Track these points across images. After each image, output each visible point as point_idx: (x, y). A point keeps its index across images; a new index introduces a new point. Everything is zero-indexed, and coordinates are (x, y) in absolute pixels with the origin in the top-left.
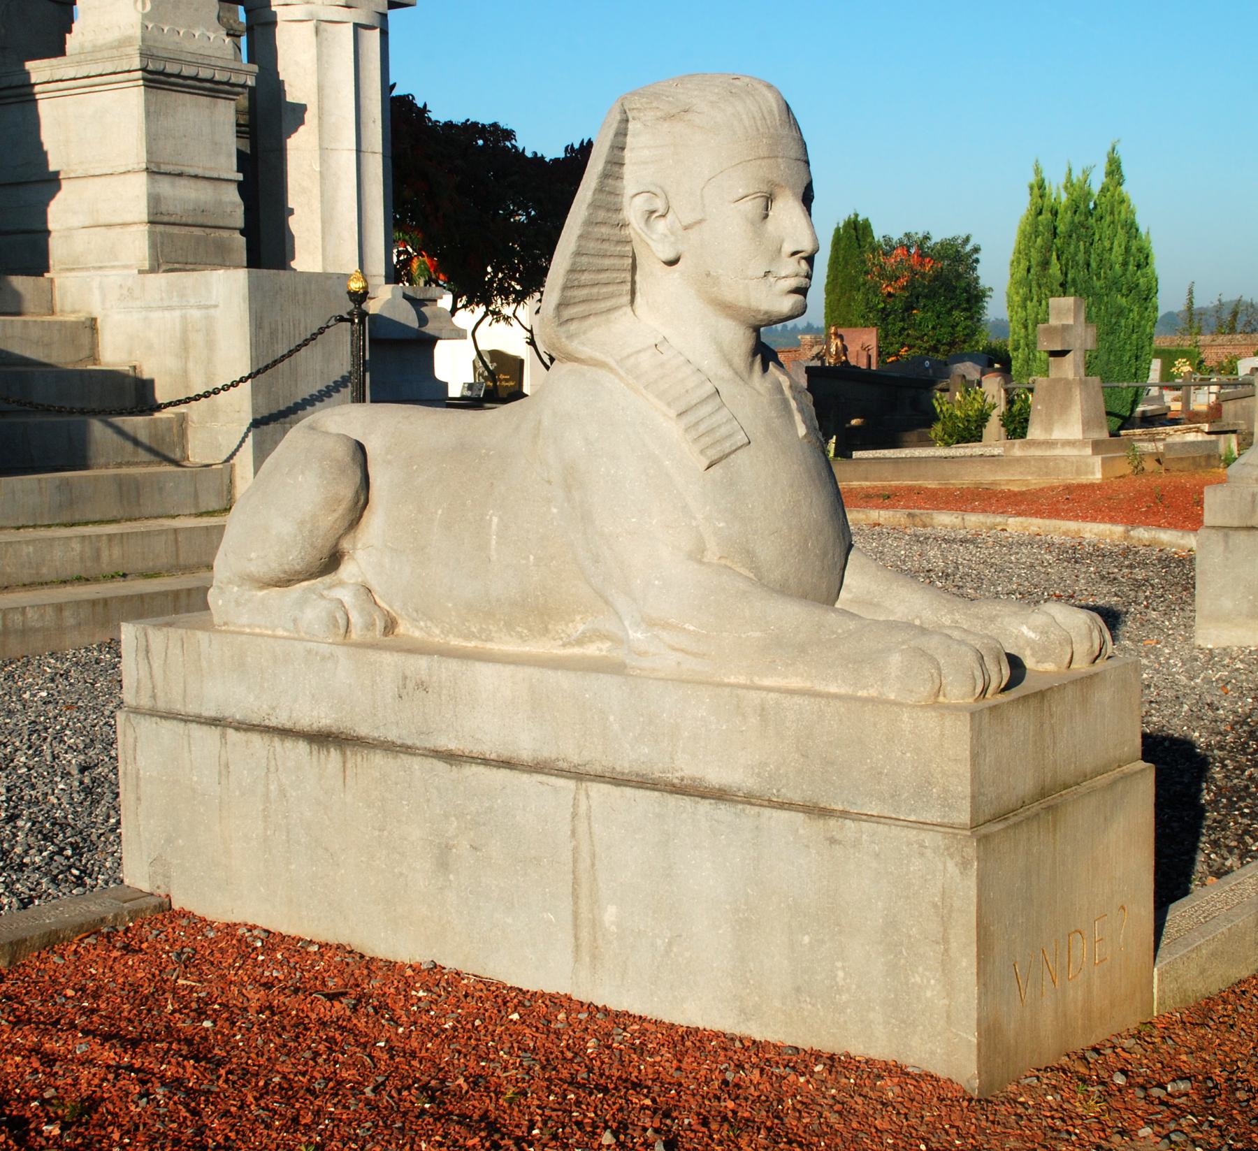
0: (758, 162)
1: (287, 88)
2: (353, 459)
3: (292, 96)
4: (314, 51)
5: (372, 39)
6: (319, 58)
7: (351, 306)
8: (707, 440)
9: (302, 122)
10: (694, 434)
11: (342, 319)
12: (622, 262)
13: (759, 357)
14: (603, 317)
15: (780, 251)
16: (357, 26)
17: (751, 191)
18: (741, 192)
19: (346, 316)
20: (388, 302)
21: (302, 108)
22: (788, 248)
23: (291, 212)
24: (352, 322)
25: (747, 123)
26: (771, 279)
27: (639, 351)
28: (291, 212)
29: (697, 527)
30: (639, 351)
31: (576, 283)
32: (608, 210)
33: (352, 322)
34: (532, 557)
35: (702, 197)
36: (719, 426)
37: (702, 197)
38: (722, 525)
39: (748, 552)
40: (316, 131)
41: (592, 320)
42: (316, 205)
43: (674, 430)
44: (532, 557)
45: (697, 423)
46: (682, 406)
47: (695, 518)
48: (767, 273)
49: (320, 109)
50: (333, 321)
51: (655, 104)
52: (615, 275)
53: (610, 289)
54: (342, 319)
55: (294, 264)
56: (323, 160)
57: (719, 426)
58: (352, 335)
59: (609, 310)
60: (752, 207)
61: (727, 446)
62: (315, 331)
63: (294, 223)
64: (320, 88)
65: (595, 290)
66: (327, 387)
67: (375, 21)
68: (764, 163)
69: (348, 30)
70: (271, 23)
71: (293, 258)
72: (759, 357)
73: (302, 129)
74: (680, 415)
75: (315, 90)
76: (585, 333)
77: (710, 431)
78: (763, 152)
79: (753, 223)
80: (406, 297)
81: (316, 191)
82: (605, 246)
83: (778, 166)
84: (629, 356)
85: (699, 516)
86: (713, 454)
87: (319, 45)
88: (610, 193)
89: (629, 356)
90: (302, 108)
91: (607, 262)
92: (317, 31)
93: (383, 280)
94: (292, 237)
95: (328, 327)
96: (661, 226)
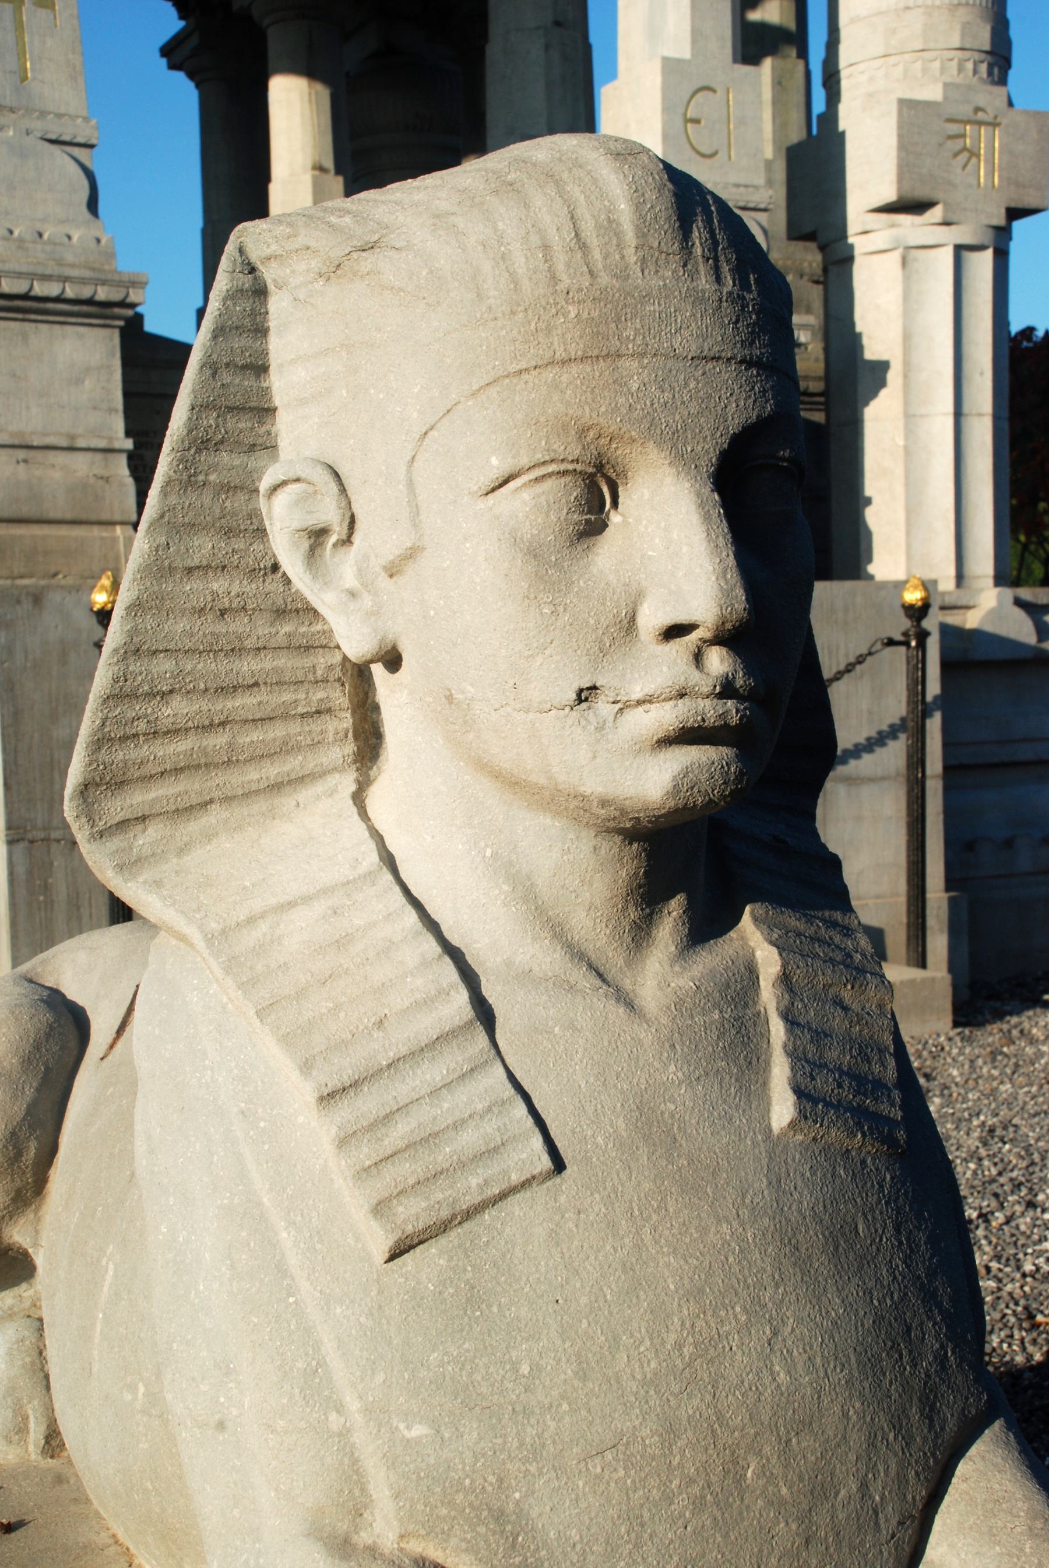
0: (549, 374)
1: (865, 341)
2: (27, 1062)
3: (872, 351)
4: (899, 290)
5: (983, 263)
6: (907, 296)
7: (906, 623)
8: (407, 1170)
9: (882, 384)
10: (365, 1153)
11: (891, 642)
12: (307, 662)
13: (676, 906)
14: (260, 805)
15: (630, 624)
16: (959, 249)
17: (525, 461)
18: (497, 465)
19: (898, 637)
20: (992, 612)
21: (883, 367)
22: (653, 617)
23: (868, 501)
24: (907, 644)
25: (519, 262)
26: (603, 707)
27: (291, 905)
28: (868, 501)
29: (344, 1433)
30: (291, 905)
31: (142, 726)
32: (229, 533)
33: (907, 644)
34: (142, 1389)
35: (410, 484)
36: (458, 1125)
37: (410, 484)
38: (418, 1431)
39: (499, 1516)
40: (901, 394)
41: (215, 815)
42: (900, 490)
43: (315, 1133)
44: (142, 1389)
45: (387, 1118)
46: (342, 1068)
47: (340, 1409)
48: (585, 695)
49: (907, 364)
50: (878, 646)
51: (301, 241)
52: (287, 697)
53: (277, 731)
54: (891, 642)
55: (871, 569)
56: (909, 431)
57: (458, 1125)
58: (908, 662)
59: (276, 787)
60: (537, 507)
61: (472, 1186)
62: (852, 660)
63: (872, 516)
64: (907, 337)
65: (218, 740)
66: (880, 733)
67: (987, 237)
68: (567, 376)
69: (946, 256)
70: (848, 259)
71: (870, 560)
72: (676, 906)
73: (883, 393)
74: (328, 1098)
75: (899, 340)
76: (181, 851)
77: (430, 1139)
78: (565, 339)
79: (534, 553)
80: (1019, 603)
81: (899, 471)
82: (237, 625)
83: (620, 383)
84: (251, 921)
85: (353, 1404)
86: (413, 1213)
87: (907, 279)
88: (229, 488)
89: (251, 921)
90: (883, 367)
91: (247, 667)
92: (904, 262)
93: (990, 582)
94: (869, 534)
95: (870, 654)
96: (345, 567)
